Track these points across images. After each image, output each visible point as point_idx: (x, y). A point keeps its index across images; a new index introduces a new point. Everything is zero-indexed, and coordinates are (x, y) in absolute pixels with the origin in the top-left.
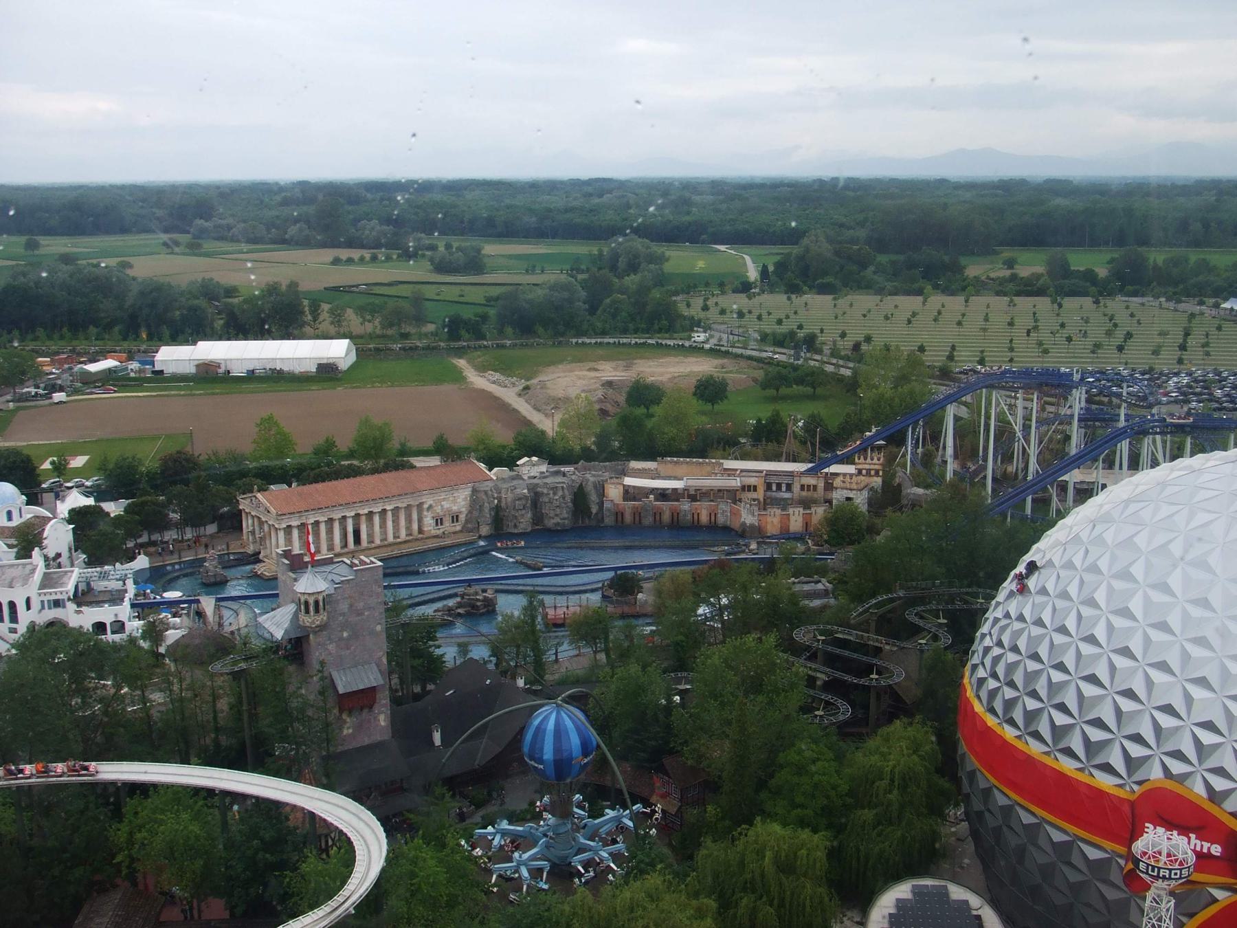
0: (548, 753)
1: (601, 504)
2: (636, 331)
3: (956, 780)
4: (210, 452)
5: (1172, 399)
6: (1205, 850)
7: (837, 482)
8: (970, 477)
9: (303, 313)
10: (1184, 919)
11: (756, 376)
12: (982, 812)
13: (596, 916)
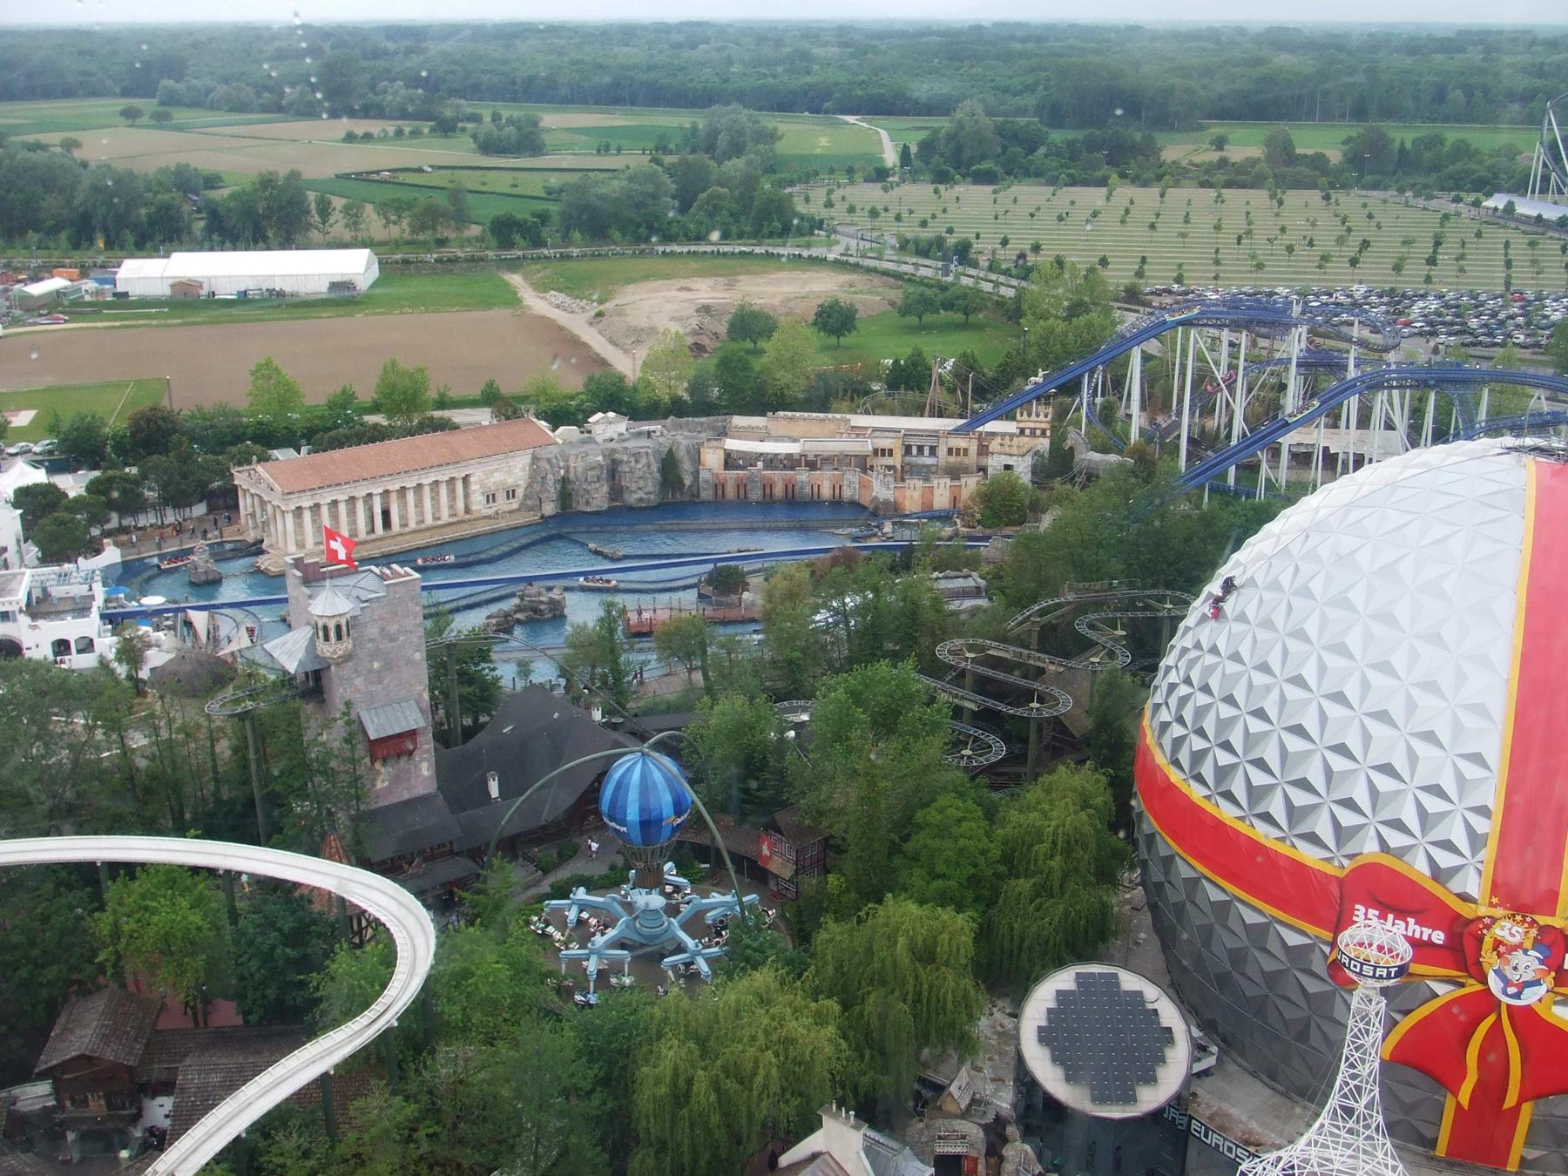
0: (633, 814)
1: (696, 474)
2: (740, 236)
3: (1131, 839)
4: (193, 408)
5: (1416, 330)
6: (1425, 938)
7: (994, 445)
9: (308, 212)
10: (1397, 1017)
11: (894, 298)
12: (1162, 883)
13: (693, 1024)
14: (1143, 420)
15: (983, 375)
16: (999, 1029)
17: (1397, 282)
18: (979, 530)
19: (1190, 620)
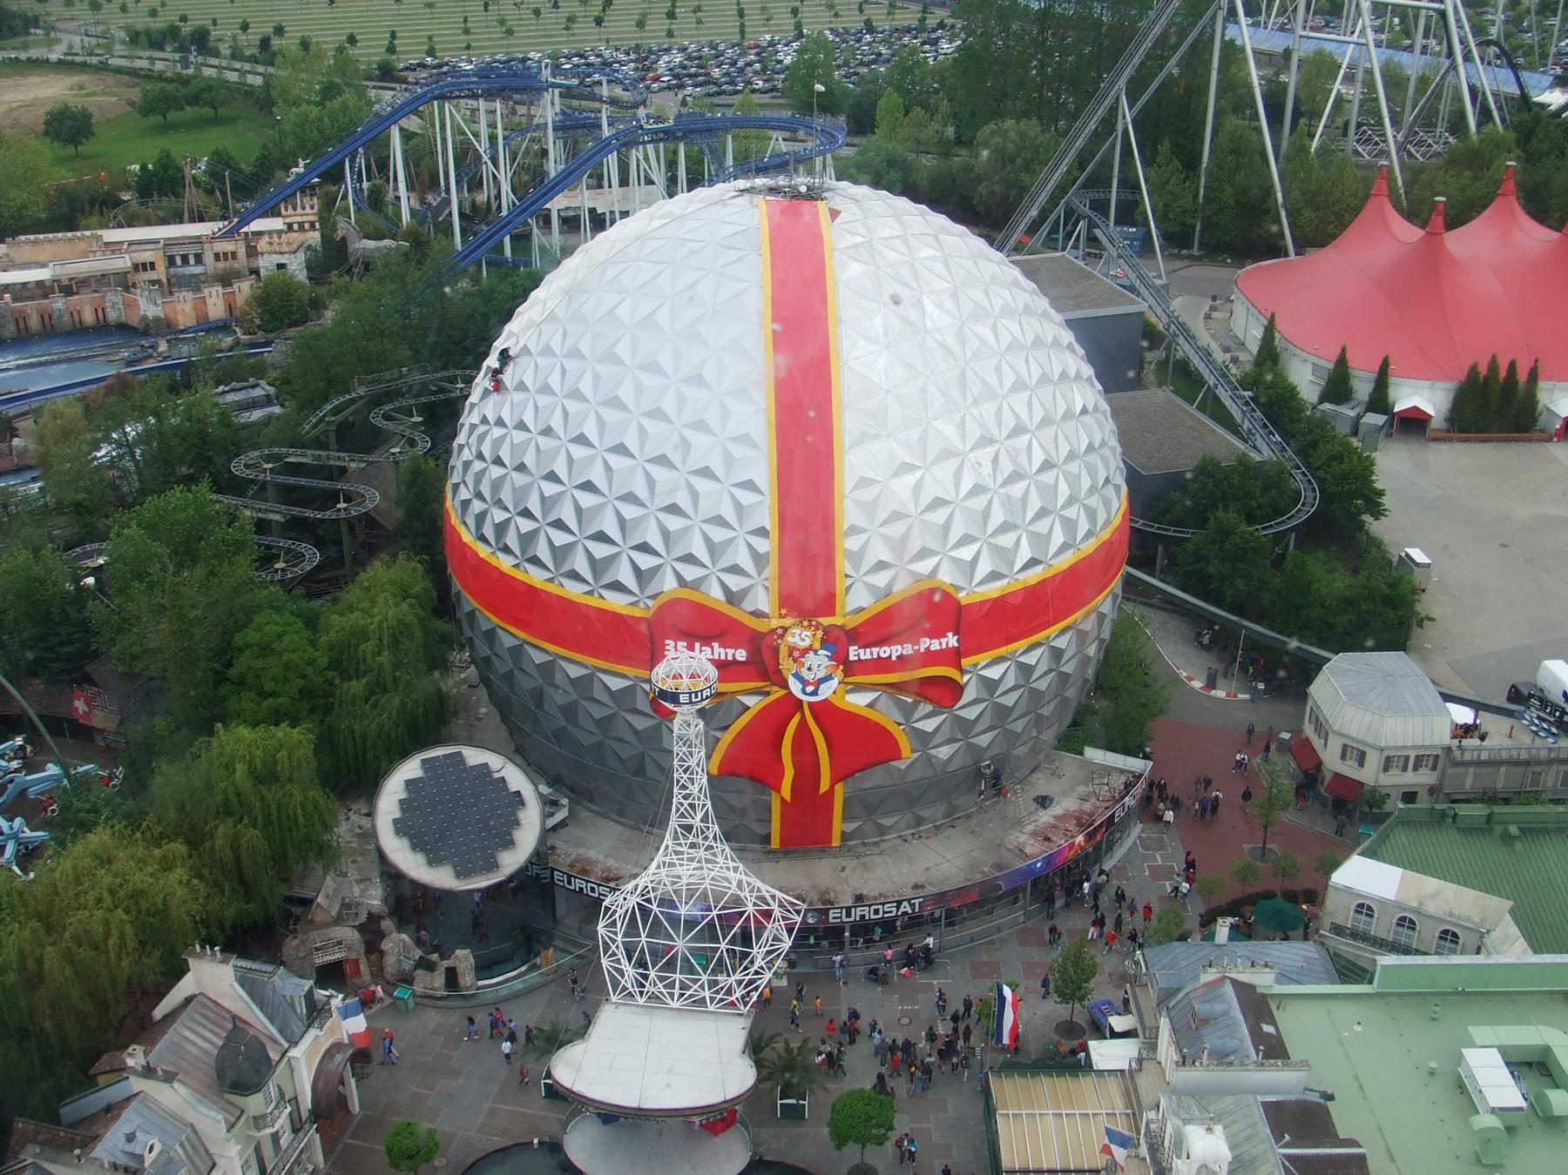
5: (664, 85)
6: (730, 658)
7: (262, 245)
8: (432, 219)
10: (718, 734)
13: (31, 902)
14: (412, 201)
15: (241, 172)
16: (358, 831)
17: (641, 38)
18: (260, 336)
19: (474, 397)
